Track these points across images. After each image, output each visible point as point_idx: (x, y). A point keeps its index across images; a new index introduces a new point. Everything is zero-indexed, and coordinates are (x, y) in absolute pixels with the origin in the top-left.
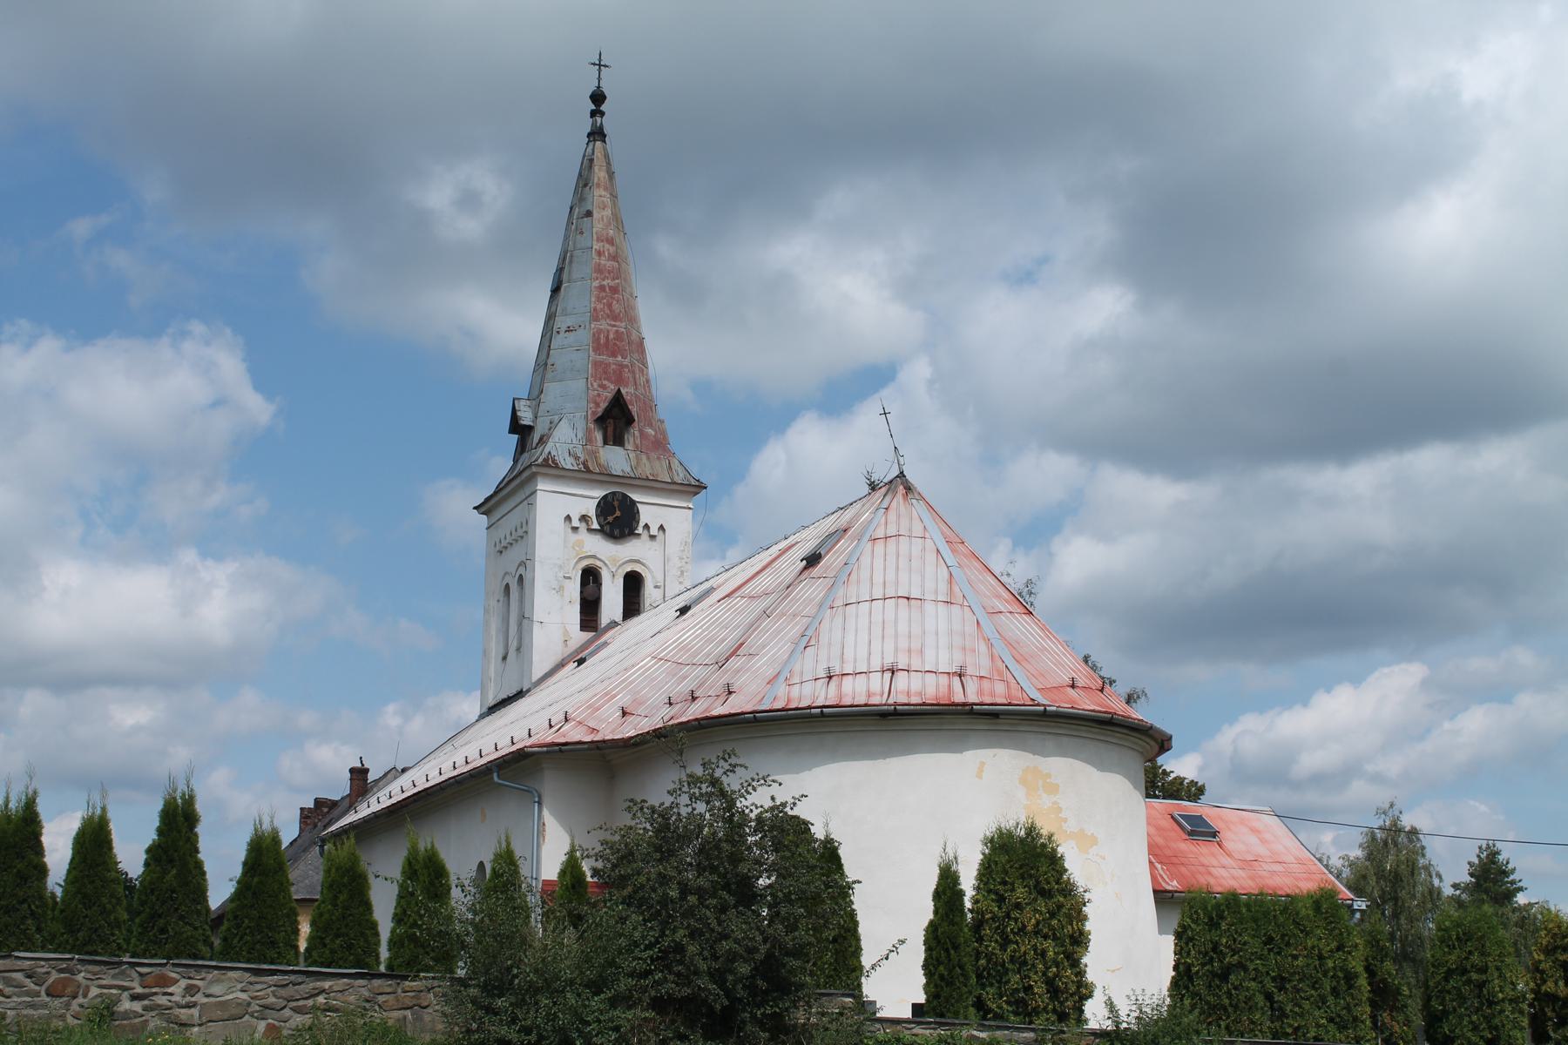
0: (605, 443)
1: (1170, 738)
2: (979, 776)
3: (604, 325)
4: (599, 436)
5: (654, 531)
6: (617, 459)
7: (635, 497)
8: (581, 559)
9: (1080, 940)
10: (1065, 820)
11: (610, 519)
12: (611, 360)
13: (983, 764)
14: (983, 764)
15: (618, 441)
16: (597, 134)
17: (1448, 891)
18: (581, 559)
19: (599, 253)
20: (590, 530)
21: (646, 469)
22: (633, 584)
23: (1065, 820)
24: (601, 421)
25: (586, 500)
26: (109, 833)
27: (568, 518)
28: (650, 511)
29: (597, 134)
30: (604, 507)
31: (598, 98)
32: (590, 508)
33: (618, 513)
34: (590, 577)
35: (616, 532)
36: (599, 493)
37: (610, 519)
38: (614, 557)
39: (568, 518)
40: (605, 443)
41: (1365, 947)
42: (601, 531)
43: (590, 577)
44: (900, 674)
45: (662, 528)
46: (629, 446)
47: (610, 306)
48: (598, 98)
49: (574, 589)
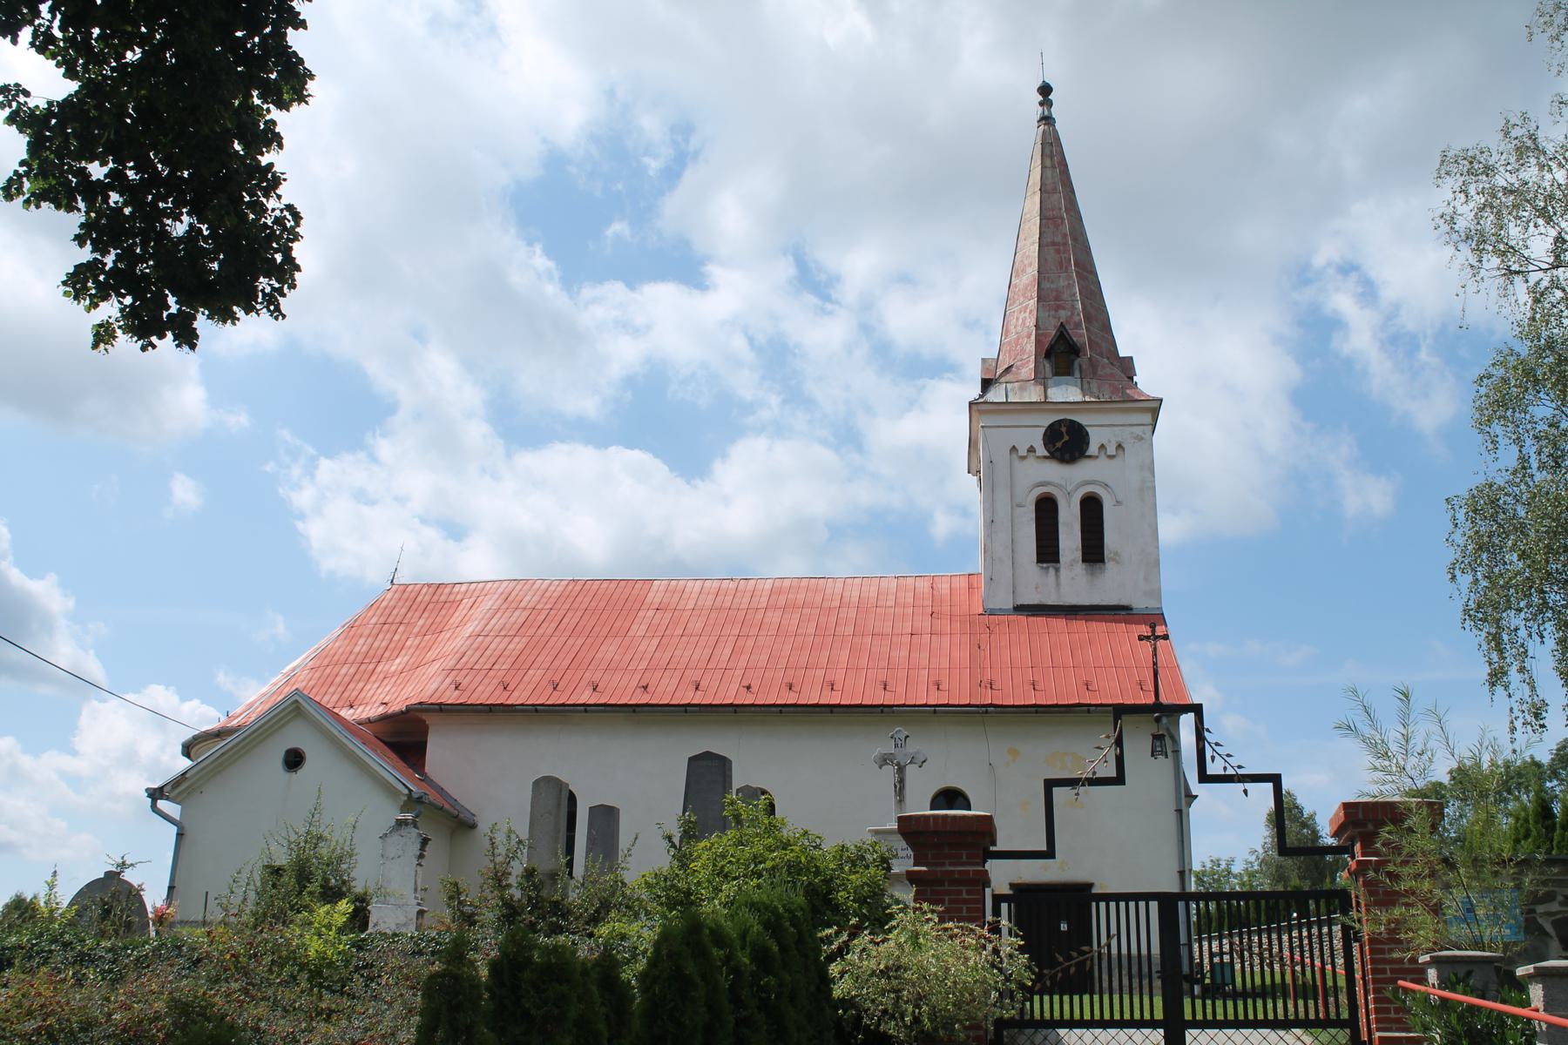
5: (1111, 450)
6: (1066, 392)
27: (1014, 449)
31: (1045, 90)
33: (1066, 438)
34: (1046, 509)
36: (1047, 420)
37: (1059, 445)
38: (1068, 482)
39: (1014, 449)
43: (1046, 509)
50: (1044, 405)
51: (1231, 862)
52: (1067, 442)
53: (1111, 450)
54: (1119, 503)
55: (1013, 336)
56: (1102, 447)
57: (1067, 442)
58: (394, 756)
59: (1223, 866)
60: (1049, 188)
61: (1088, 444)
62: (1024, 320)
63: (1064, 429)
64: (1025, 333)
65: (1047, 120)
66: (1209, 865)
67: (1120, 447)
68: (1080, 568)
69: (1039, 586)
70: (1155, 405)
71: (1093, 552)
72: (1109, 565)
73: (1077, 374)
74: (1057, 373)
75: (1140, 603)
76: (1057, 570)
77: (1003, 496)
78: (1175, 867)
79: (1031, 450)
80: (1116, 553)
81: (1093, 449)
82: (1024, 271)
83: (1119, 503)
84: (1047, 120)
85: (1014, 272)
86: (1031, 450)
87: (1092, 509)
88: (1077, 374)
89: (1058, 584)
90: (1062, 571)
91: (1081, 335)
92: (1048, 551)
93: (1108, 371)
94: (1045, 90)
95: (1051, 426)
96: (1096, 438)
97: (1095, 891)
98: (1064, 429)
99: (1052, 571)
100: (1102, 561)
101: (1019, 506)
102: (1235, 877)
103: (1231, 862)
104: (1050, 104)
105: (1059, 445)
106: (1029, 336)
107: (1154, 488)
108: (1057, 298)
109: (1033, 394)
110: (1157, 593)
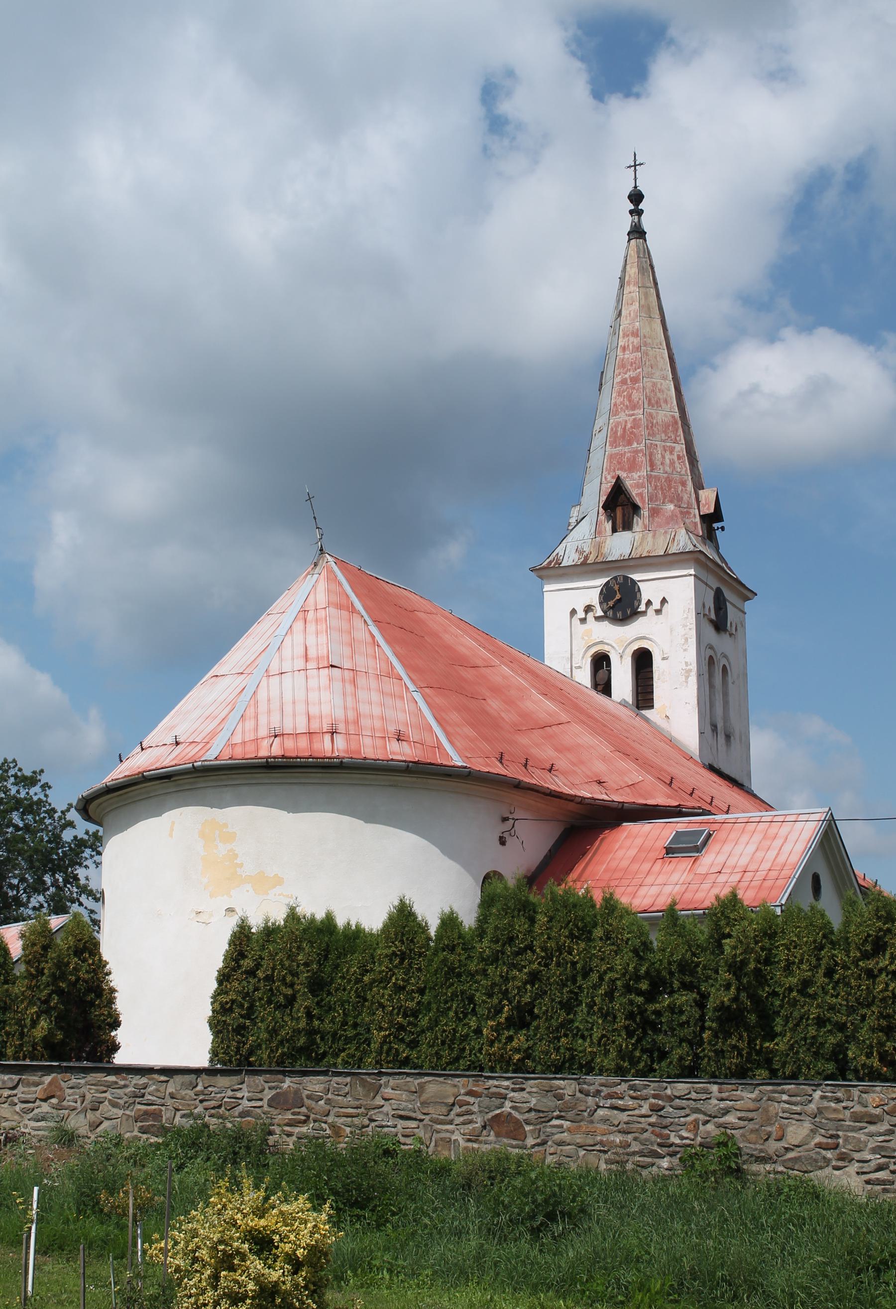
0: (614, 530)
2: (171, 835)
3: (622, 417)
4: (608, 526)
6: (620, 545)
7: (636, 577)
8: (589, 647)
10: (241, 865)
11: (611, 603)
12: (627, 449)
13: (173, 823)
14: (173, 823)
15: (627, 526)
16: (637, 232)
18: (589, 647)
19: (624, 349)
20: (597, 619)
22: (643, 661)
23: (241, 865)
25: (588, 592)
26: (99, 968)
29: (637, 232)
30: (606, 594)
31: (636, 197)
32: (593, 597)
33: (618, 596)
35: (619, 615)
40: (614, 530)
41: (49, 976)
43: (601, 662)
44: (314, 736)
45: (664, 601)
46: (636, 528)
47: (629, 397)
48: (636, 197)
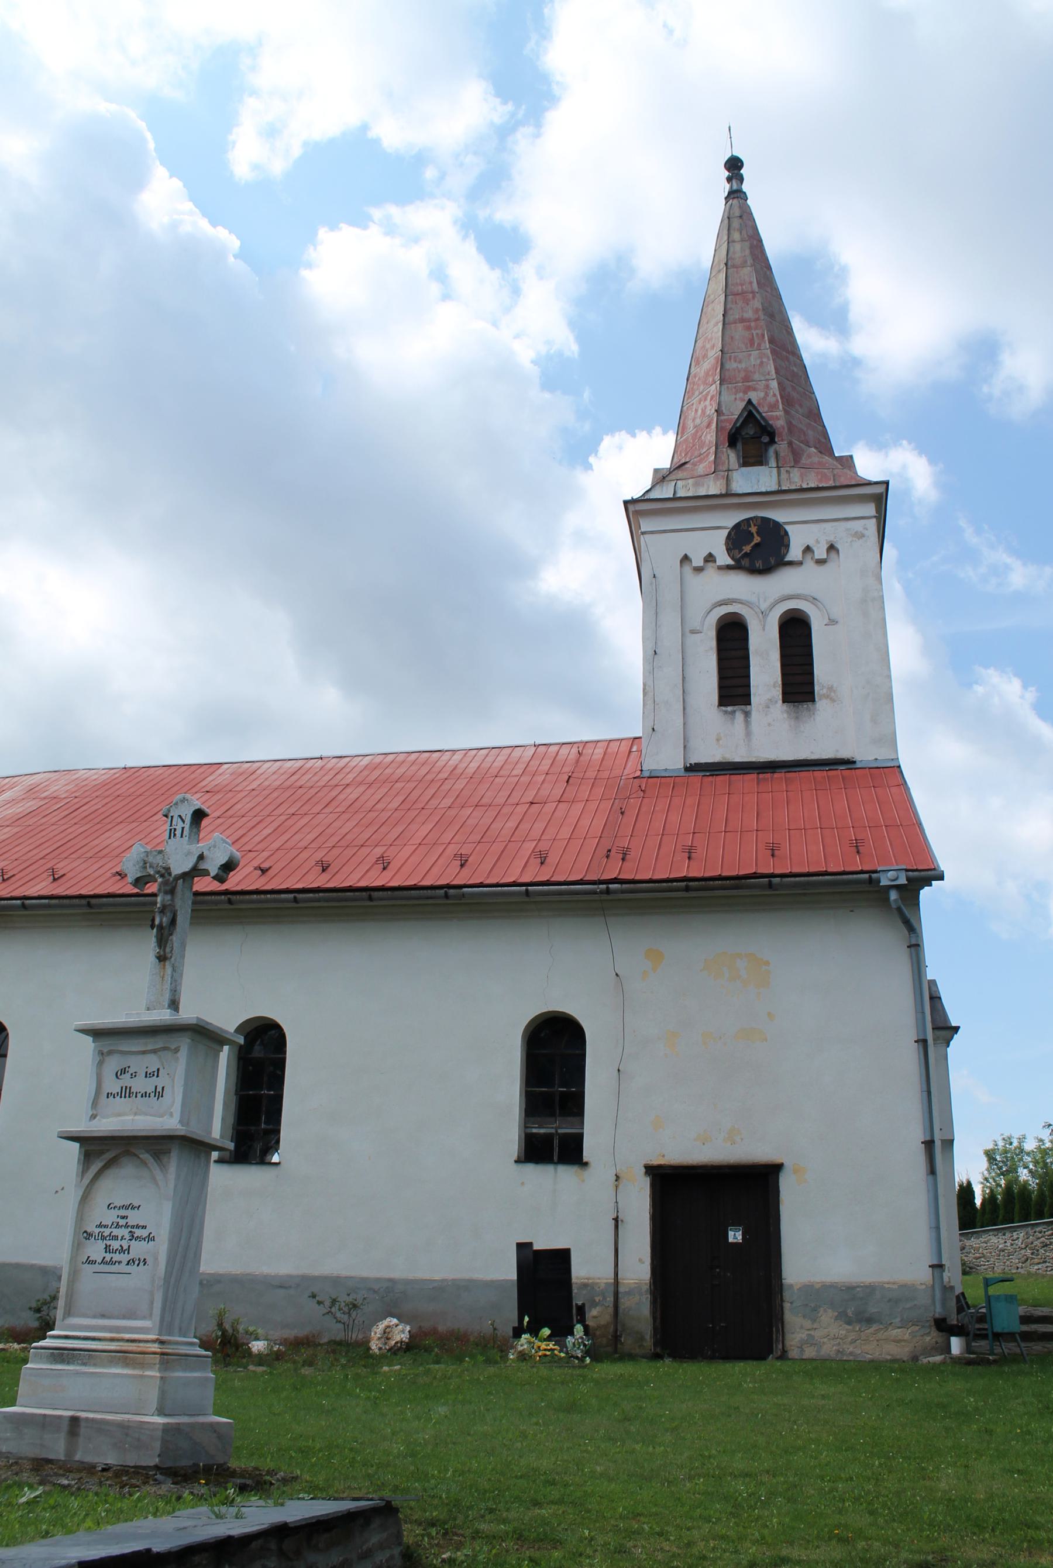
1: (656, 471)
5: (820, 553)
6: (761, 479)
9: (230, 1537)
17: (1033, 689)
21: (796, 479)
24: (733, 439)
27: (686, 559)
28: (803, 532)
30: (737, 538)
31: (734, 165)
32: (717, 544)
33: (757, 539)
34: (732, 635)
36: (731, 519)
37: (747, 549)
38: (761, 599)
39: (686, 559)
42: (737, 566)
43: (732, 635)
49: (824, 669)
50: (727, 499)
51: (1022, 1139)
52: (759, 548)
53: (820, 553)
54: (832, 622)
55: (691, 429)
56: (808, 549)
57: (759, 548)
58: (524, 1106)
59: (1015, 1144)
60: (738, 262)
61: (788, 546)
62: (704, 412)
63: (753, 529)
64: (706, 421)
65: (736, 195)
66: (1001, 1144)
67: (832, 548)
68: (779, 709)
69: (722, 738)
70: (880, 489)
71: (799, 686)
72: (822, 705)
73: (773, 463)
74: (745, 463)
75: (865, 754)
76: (747, 714)
77: (671, 621)
78: (917, 1135)
79: (710, 558)
80: (831, 688)
81: (795, 553)
82: (705, 356)
83: (832, 622)
84: (736, 195)
85: (695, 360)
86: (710, 558)
87: (795, 631)
88: (773, 463)
89: (748, 734)
90: (755, 715)
91: (777, 418)
92: (734, 690)
93: (816, 459)
94: (734, 165)
95: (737, 526)
96: (798, 539)
97: (516, 1325)
98: (753, 529)
99: (739, 717)
100: (813, 700)
101: (693, 632)
102: (1028, 1154)
103: (1022, 1139)
104: (741, 179)
105: (747, 549)
106: (709, 426)
107: (882, 598)
108: (747, 379)
109: (714, 487)
110: (892, 742)
